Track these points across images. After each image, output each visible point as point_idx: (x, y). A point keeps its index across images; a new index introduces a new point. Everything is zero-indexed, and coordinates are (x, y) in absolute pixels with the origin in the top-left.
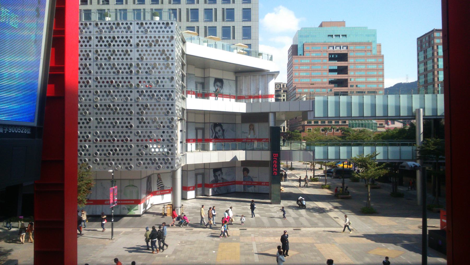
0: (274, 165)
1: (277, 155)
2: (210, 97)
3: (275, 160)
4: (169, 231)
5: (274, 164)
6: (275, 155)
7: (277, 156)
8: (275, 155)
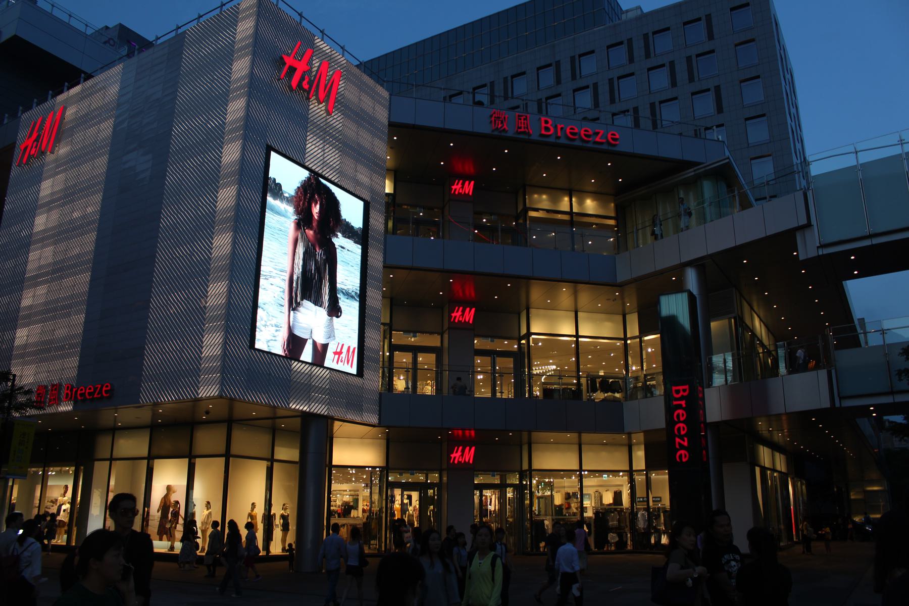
0: (676, 427)
1: (684, 390)
2: (149, 533)
3: (679, 407)
4: (595, 503)
5: (677, 423)
6: (678, 392)
7: (686, 394)
8: (678, 392)
